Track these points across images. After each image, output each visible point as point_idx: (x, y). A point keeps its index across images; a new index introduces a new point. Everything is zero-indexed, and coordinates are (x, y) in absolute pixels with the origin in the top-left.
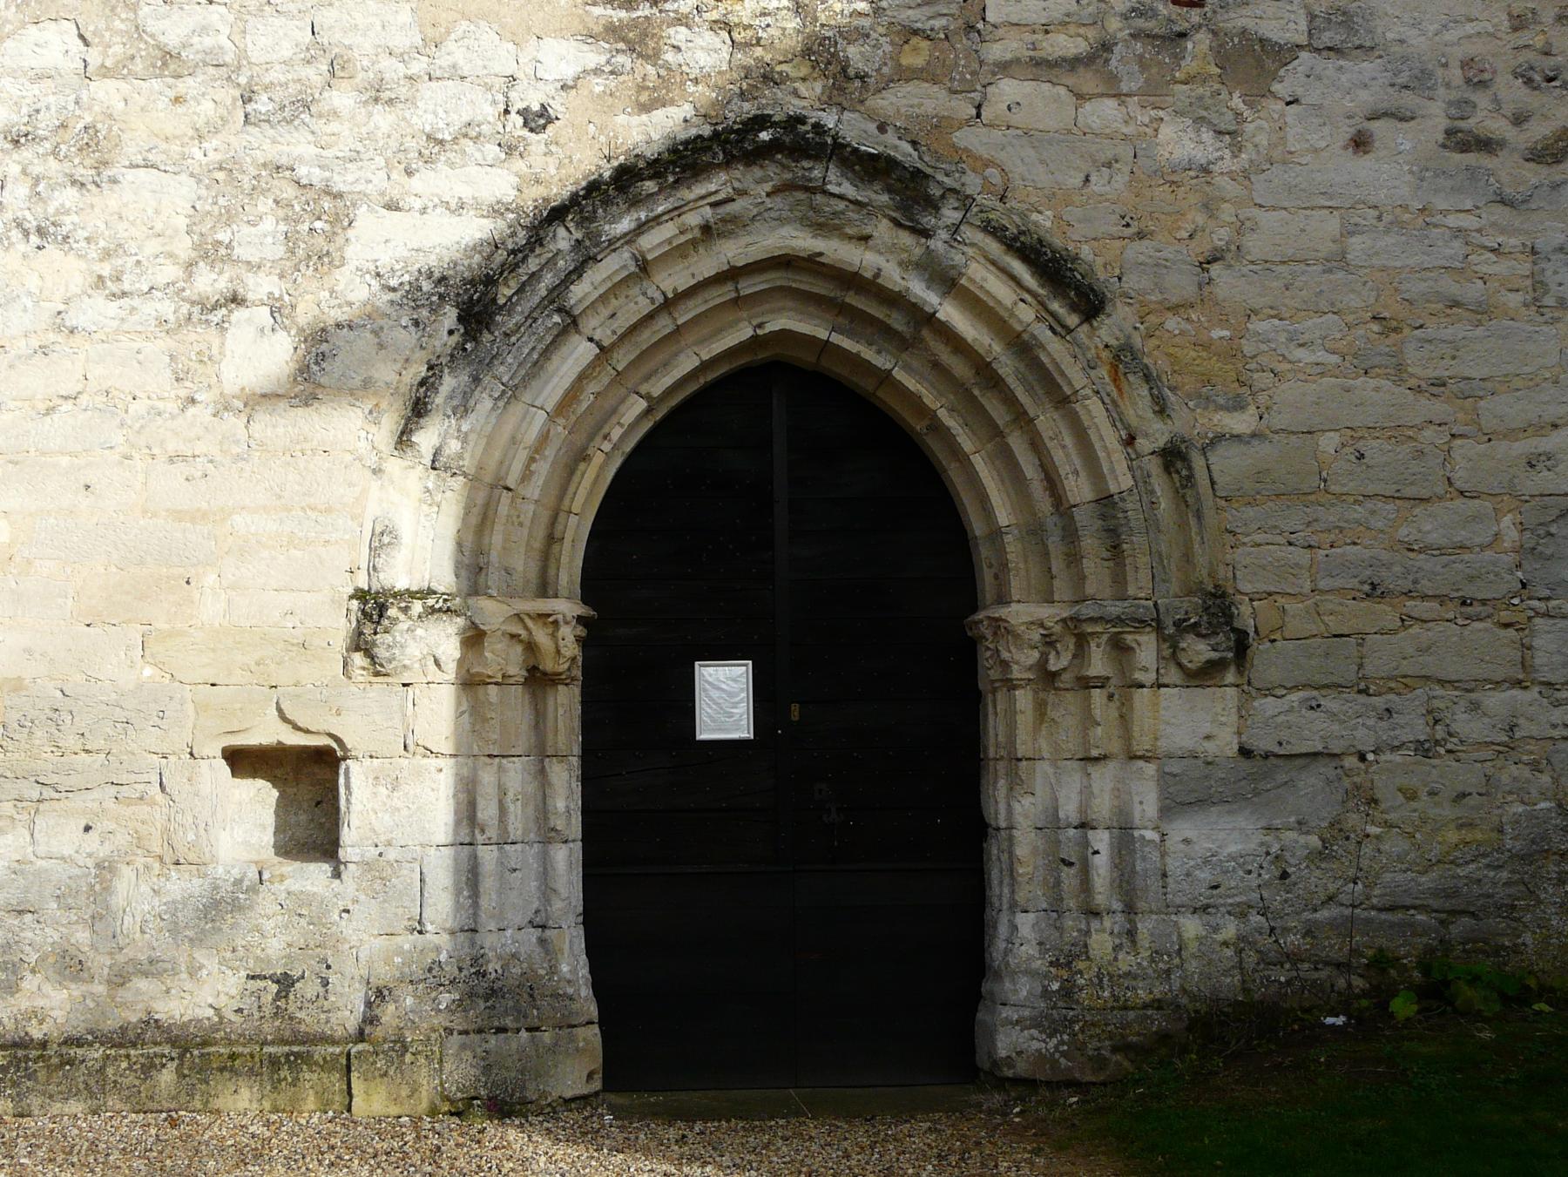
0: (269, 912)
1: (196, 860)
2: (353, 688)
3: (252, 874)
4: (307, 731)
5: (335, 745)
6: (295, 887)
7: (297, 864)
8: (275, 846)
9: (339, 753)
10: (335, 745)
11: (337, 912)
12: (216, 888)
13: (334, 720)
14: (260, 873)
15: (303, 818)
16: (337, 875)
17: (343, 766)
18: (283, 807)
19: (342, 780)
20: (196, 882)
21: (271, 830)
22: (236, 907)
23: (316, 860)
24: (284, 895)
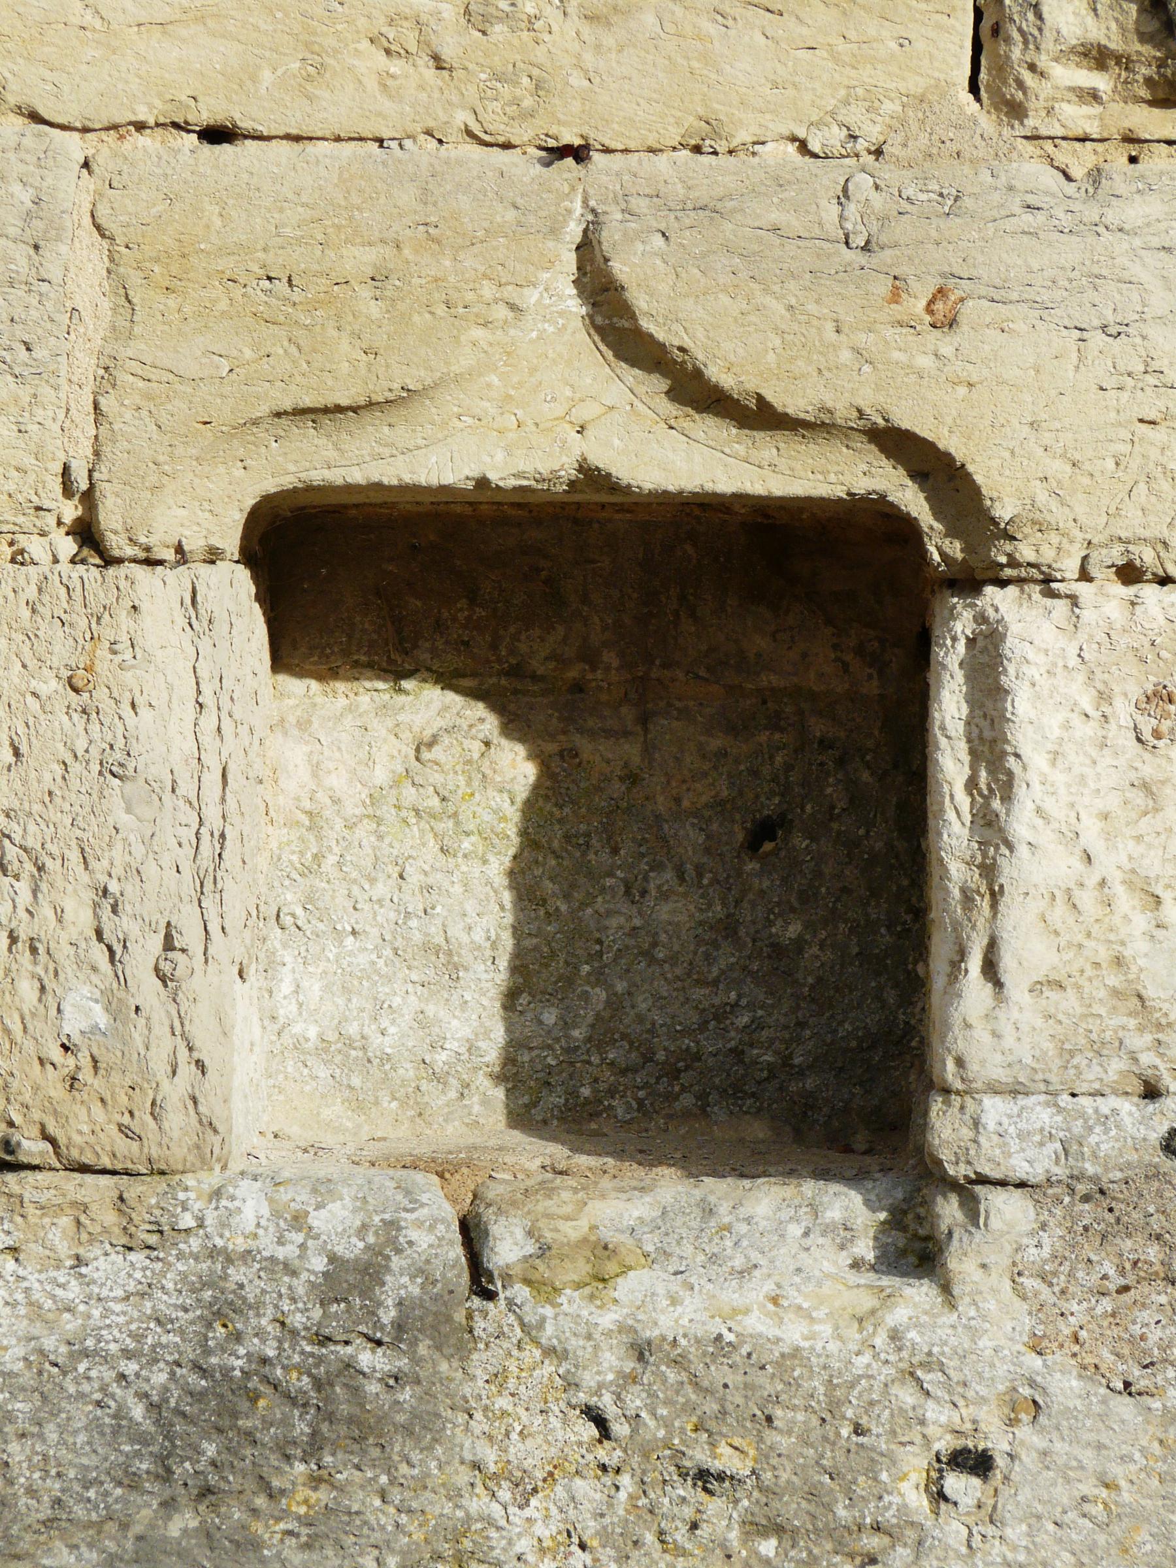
0: (530, 1455)
1: (111, 1146)
2: (1030, 170)
3: (432, 1238)
4: (760, 417)
5: (912, 500)
6: (681, 1316)
7: (670, 1187)
8: (512, 1073)
9: (941, 546)
10: (912, 500)
11: (915, 1465)
12: (225, 1310)
13: (924, 351)
14: (472, 1233)
15: (675, 913)
16: (914, 1251)
17: (961, 622)
18: (557, 854)
19: (951, 706)
20: (112, 1269)
21: (488, 979)
22: (339, 1420)
23: (748, 1163)
24: (613, 1360)
